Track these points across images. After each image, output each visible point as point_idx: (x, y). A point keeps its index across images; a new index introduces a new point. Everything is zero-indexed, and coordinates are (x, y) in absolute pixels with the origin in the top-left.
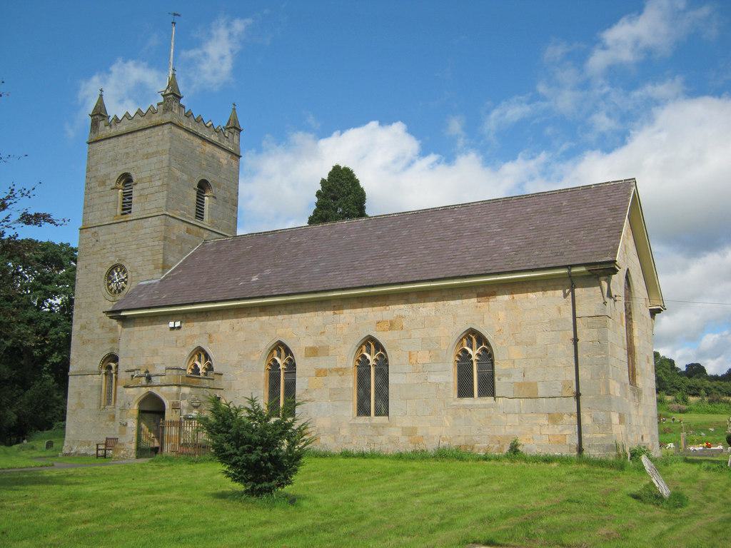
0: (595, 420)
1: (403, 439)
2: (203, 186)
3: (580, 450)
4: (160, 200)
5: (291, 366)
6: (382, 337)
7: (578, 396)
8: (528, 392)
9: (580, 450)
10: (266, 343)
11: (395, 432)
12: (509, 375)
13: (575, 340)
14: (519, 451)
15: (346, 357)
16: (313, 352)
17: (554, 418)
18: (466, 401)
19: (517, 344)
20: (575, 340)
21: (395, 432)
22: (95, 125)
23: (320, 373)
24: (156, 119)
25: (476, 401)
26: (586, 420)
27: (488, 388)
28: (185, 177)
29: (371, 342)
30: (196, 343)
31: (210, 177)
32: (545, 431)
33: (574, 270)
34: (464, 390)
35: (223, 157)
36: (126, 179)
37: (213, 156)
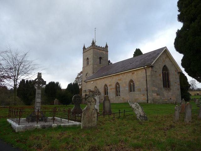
0: (150, 95)
1: (122, 100)
2: (100, 58)
3: (148, 100)
4: (92, 62)
5: (107, 88)
6: (119, 82)
7: (147, 90)
8: (139, 90)
9: (148, 100)
10: (104, 85)
11: (121, 99)
12: (137, 87)
13: (146, 80)
14: (73, 88)
15: (114, 86)
16: (110, 85)
17: (144, 95)
18: (131, 92)
19: (138, 81)
20: (146, 80)
21: (121, 99)
22: (83, 50)
23: (111, 89)
24: (91, 48)
25: (132, 92)
26: (149, 95)
27: (134, 91)
28: (96, 57)
29: (131, 81)
30: (95, 85)
31: (102, 56)
32: (142, 97)
33: (143, 67)
34: (130, 91)
35: (104, 52)
36: (88, 59)
37: (102, 53)
